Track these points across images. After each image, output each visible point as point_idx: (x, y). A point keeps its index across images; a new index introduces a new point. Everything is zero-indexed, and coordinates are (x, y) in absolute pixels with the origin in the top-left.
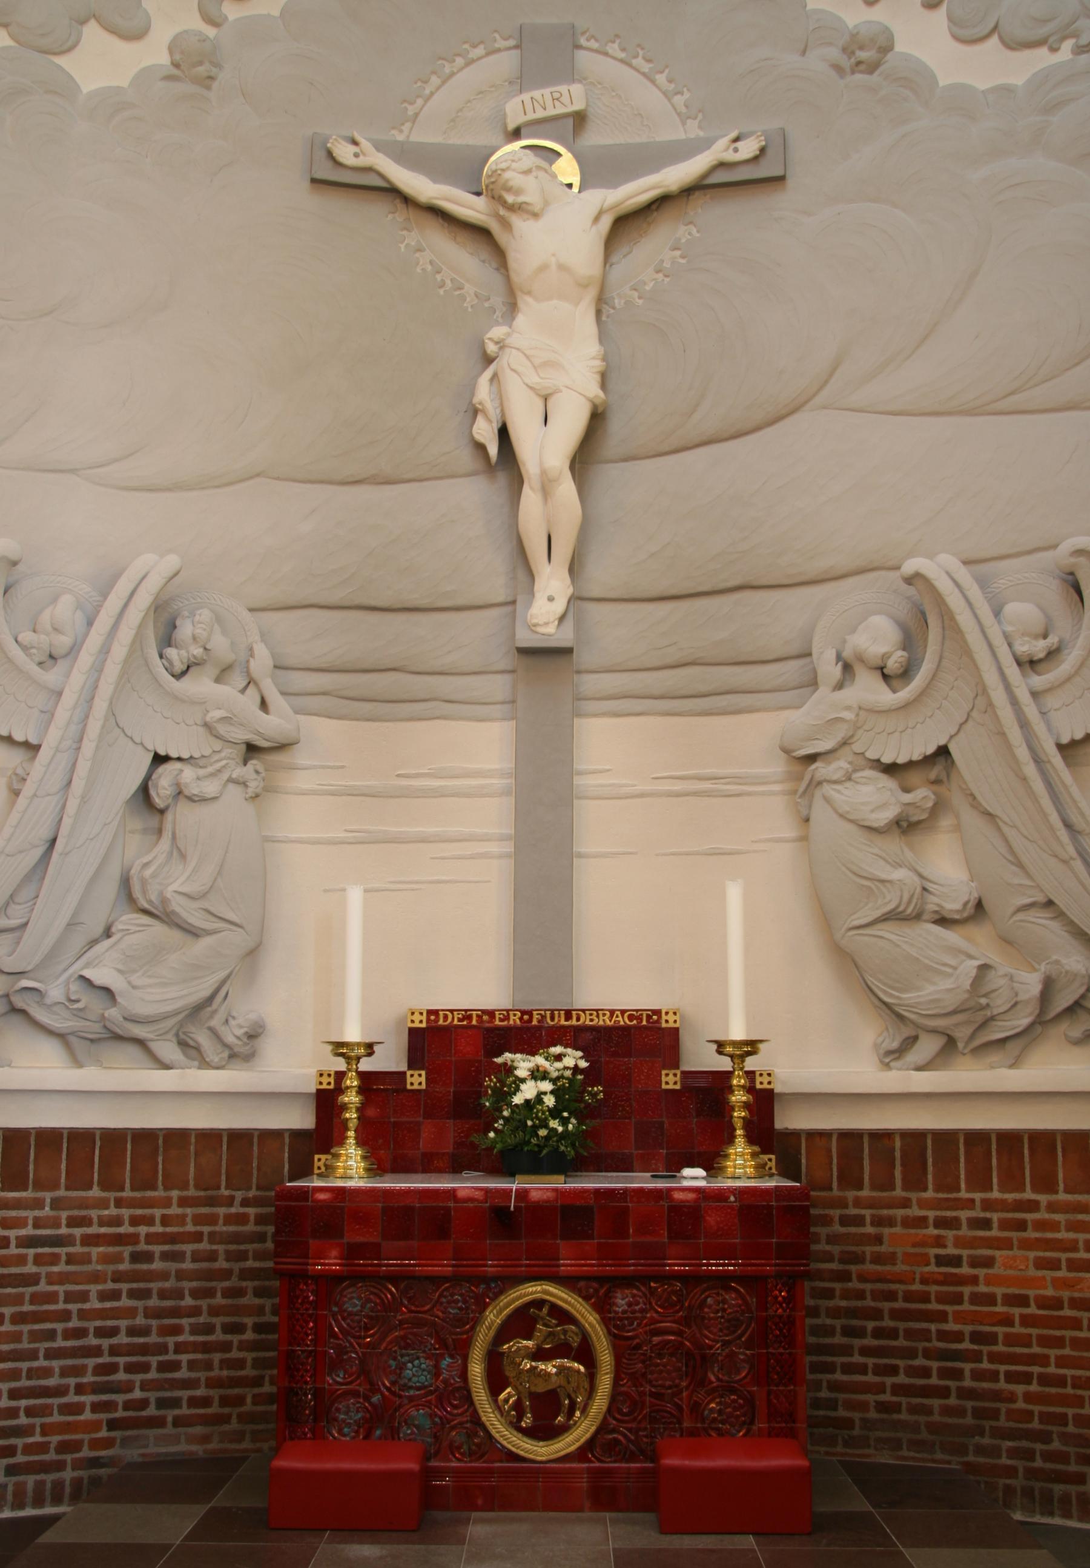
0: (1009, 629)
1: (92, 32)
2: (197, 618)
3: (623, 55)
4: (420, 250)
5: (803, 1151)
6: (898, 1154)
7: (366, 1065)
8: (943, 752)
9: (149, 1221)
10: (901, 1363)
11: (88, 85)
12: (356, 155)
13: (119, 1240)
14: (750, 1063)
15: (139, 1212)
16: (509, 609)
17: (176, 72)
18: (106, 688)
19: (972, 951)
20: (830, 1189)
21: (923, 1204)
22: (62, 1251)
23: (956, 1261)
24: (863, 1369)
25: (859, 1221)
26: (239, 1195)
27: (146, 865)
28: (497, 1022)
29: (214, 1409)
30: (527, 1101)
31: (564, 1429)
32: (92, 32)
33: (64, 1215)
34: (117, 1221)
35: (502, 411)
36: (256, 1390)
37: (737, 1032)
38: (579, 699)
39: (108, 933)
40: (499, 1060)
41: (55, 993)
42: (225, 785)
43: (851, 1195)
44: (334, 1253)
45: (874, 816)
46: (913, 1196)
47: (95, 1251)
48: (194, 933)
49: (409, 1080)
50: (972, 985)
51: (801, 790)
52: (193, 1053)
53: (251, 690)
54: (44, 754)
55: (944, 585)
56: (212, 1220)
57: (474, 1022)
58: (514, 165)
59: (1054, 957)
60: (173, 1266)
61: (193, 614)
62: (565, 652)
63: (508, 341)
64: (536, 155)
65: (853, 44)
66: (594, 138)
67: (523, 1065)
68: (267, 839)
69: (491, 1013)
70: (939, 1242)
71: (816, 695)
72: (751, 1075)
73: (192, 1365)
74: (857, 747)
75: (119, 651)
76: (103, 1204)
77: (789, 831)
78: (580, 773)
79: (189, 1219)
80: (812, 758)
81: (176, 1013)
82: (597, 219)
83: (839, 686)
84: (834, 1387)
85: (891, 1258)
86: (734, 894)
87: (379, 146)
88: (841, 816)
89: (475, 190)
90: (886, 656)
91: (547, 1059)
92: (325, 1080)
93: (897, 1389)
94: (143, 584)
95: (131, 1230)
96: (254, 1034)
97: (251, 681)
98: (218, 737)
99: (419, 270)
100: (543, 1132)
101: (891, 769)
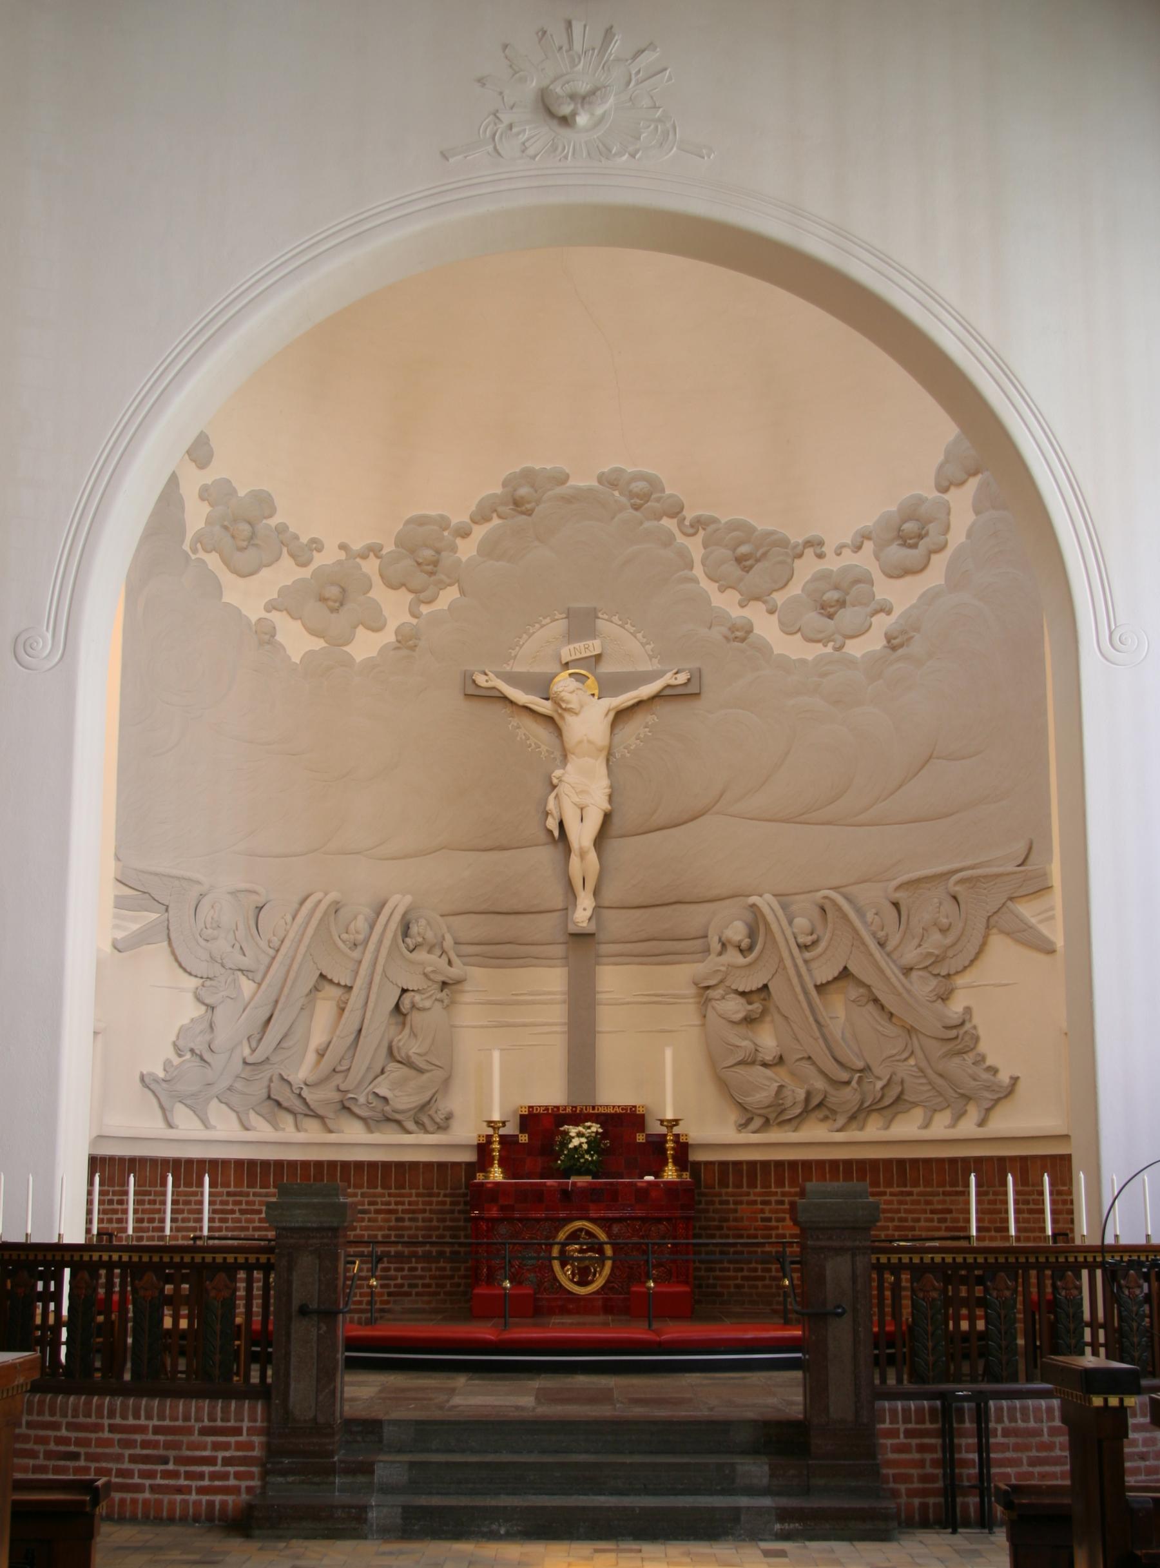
0: (795, 930)
1: (361, 631)
2: (419, 924)
3: (620, 623)
4: (519, 728)
5: (702, 1171)
6: (745, 1172)
7: (502, 1131)
8: (765, 986)
9: (403, 1203)
10: (745, 1266)
11: (358, 659)
12: (487, 681)
13: (390, 1212)
14: (676, 1130)
15: (399, 1199)
16: (564, 912)
17: (399, 645)
18: (381, 961)
19: (777, 1078)
20: (715, 1188)
21: (755, 1194)
22: (366, 1216)
23: (769, 1220)
24: (728, 1270)
25: (727, 1202)
26: (442, 1192)
27: (399, 1041)
28: (561, 1111)
29: (433, 1289)
30: (575, 1147)
31: (592, 1282)
32: (361, 631)
33: (366, 1200)
34: (389, 1203)
35: (561, 813)
36: (452, 1281)
37: (669, 1115)
38: (598, 957)
39: (383, 1072)
40: (562, 1129)
41: (362, 1100)
42: (433, 1003)
43: (724, 1191)
44: (495, 1209)
45: (734, 1016)
46: (751, 1191)
47: (380, 1216)
48: (421, 1071)
49: (520, 1138)
50: (776, 1095)
51: (702, 1002)
52: (421, 1126)
53: (444, 956)
54: (355, 991)
55: (766, 910)
56: (430, 1203)
57: (550, 1111)
58: (566, 689)
59: (811, 1082)
60: (413, 1224)
61: (417, 922)
62: (592, 935)
63: (563, 778)
64: (577, 681)
65: (733, 629)
66: (605, 668)
67: (573, 1131)
68: (453, 1026)
69: (558, 1107)
70: (762, 1211)
71: (709, 958)
72: (677, 1136)
73: (423, 1269)
74: (727, 984)
75: (387, 942)
76: (383, 1195)
77: (697, 1021)
78: (598, 993)
79: (420, 1203)
80: (708, 988)
81: (414, 1108)
82: (607, 714)
83: (720, 954)
84: (716, 1278)
85: (742, 1219)
86: (669, 1054)
87: (498, 675)
88: (720, 1016)
89: (545, 696)
90: (740, 941)
91: (584, 1128)
92: (523, 1109)
93: (743, 1278)
94: (395, 911)
95: (395, 1207)
96: (449, 1117)
97: (444, 952)
98: (430, 979)
99: (518, 739)
100: (582, 1160)
101: (743, 994)
